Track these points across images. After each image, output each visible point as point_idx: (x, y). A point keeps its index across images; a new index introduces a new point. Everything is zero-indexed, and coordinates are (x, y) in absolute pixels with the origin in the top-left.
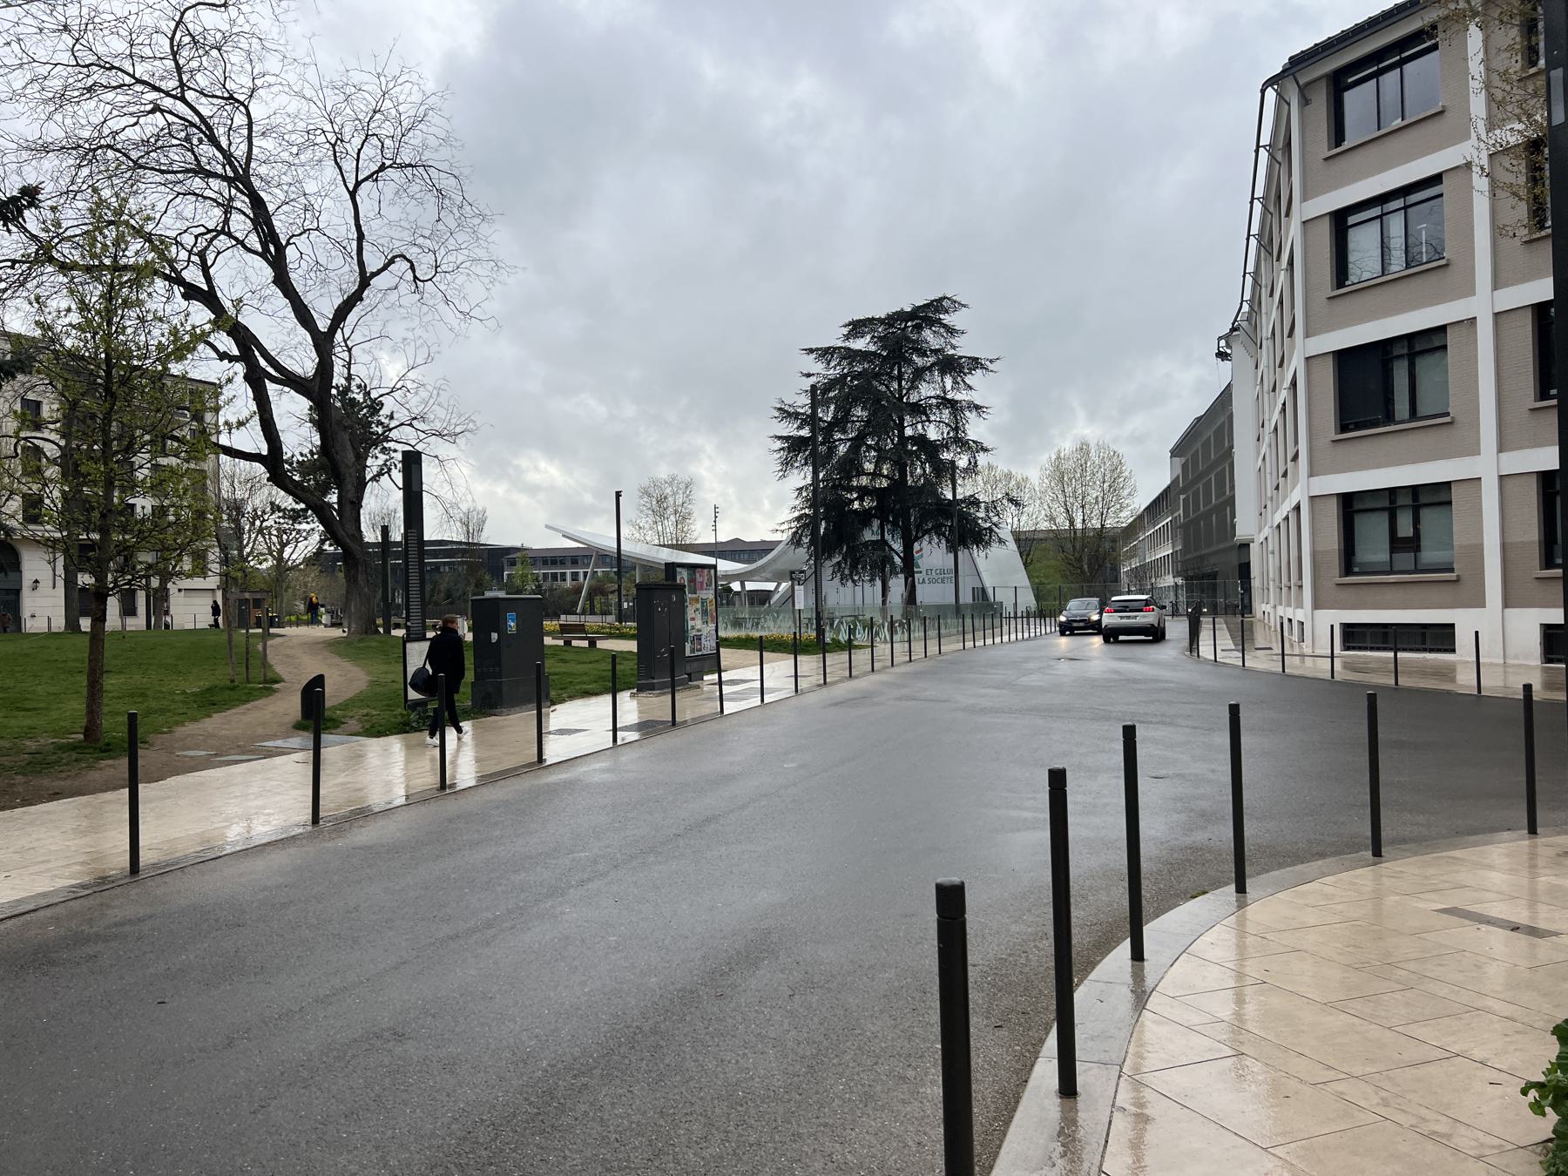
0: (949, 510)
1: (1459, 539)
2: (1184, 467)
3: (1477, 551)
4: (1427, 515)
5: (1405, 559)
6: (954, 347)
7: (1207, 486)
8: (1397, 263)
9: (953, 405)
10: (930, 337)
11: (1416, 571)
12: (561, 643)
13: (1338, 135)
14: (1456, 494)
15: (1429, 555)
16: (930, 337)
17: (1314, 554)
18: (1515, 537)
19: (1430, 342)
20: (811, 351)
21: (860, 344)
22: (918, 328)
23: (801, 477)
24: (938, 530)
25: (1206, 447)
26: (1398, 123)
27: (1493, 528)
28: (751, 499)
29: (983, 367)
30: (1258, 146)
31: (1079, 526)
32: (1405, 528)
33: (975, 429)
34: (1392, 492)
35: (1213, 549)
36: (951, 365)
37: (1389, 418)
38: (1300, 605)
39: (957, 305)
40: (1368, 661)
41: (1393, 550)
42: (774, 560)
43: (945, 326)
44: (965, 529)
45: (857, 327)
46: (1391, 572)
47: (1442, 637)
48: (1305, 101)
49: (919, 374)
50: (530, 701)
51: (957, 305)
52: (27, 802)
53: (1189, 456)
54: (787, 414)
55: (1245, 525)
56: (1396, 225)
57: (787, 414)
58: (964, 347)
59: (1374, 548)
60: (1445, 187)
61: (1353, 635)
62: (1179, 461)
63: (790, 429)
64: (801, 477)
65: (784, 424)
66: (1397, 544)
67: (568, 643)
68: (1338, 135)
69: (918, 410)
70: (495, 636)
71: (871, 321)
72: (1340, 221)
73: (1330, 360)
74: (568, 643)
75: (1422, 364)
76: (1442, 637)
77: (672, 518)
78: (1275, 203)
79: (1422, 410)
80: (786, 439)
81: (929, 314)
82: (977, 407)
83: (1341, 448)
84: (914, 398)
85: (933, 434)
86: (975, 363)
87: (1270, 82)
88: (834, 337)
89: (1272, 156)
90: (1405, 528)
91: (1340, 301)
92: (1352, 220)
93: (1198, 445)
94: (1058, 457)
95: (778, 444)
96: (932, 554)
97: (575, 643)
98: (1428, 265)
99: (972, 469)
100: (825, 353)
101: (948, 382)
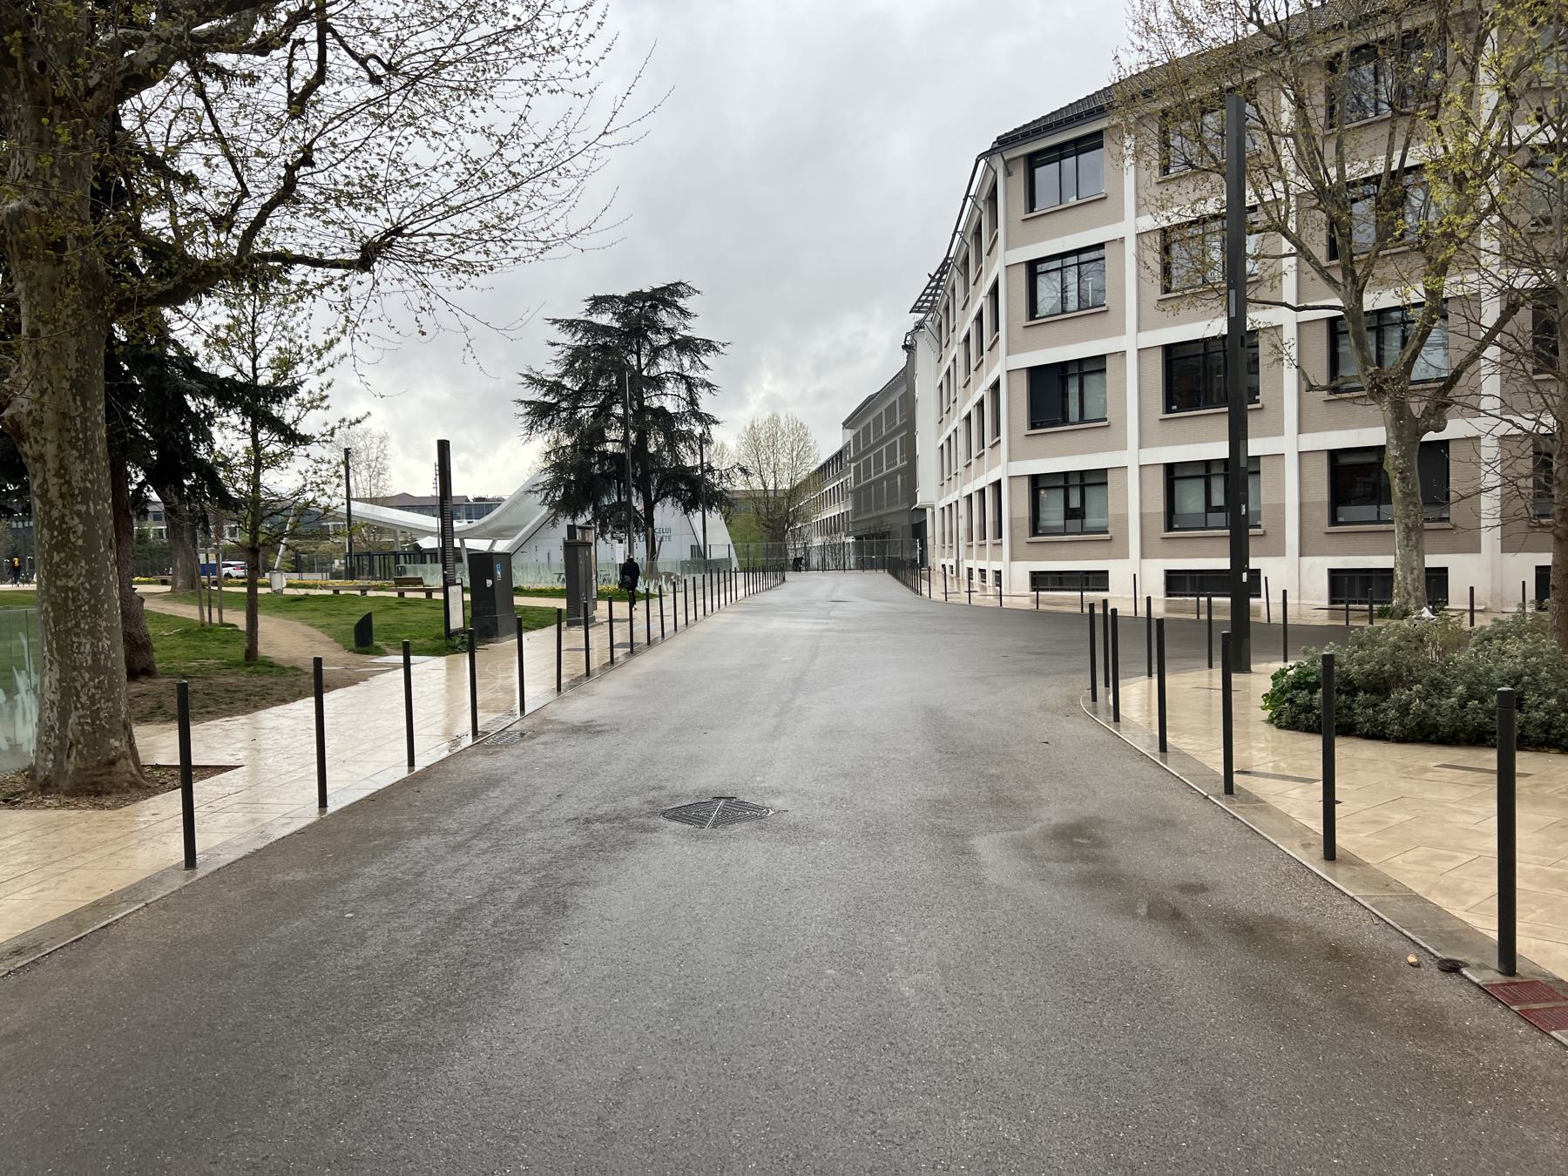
0: (684, 474)
1: (1112, 509)
2: (856, 437)
3: (1124, 520)
4: (1089, 492)
5: (1074, 524)
6: (685, 328)
7: (878, 457)
8: (1073, 304)
9: (690, 385)
10: (665, 317)
11: (1082, 533)
12: (396, 594)
13: (1031, 205)
14: (1110, 477)
15: (1092, 521)
16: (665, 317)
17: (1011, 520)
18: (1148, 509)
19: (1097, 364)
20: (555, 321)
21: (605, 319)
22: (654, 307)
23: (541, 443)
24: (676, 493)
25: (885, 421)
26: (1073, 200)
27: (1133, 501)
28: (509, 464)
29: (715, 349)
30: (967, 195)
31: (771, 487)
32: (1075, 502)
33: (706, 403)
34: (1066, 474)
35: (894, 509)
36: (687, 345)
37: (1065, 420)
38: (1000, 559)
39: (692, 291)
40: (1053, 598)
41: (1067, 517)
42: (496, 518)
43: (678, 308)
44: (696, 492)
45: (598, 303)
46: (1065, 533)
47: (1098, 580)
48: (1008, 174)
49: (656, 352)
50: (509, 632)
51: (692, 291)
52: (284, 701)
53: (860, 428)
54: (533, 381)
55: (928, 492)
56: (1072, 277)
57: (533, 381)
58: (697, 329)
59: (1053, 513)
60: (1105, 252)
61: (1039, 581)
62: (850, 434)
63: (537, 395)
64: (541, 443)
65: (530, 390)
66: (1071, 514)
67: (401, 595)
68: (1031, 205)
69: (657, 383)
70: (489, 582)
71: (609, 299)
72: (1032, 267)
73: (1025, 373)
74: (401, 595)
75: (1091, 381)
76: (1098, 580)
77: (365, 473)
78: (976, 236)
79: (1089, 415)
80: (530, 403)
81: (665, 296)
82: (709, 385)
83: (1030, 441)
84: (654, 372)
85: (671, 408)
86: (709, 346)
87: (983, 156)
88: (578, 311)
89: (975, 204)
90: (1075, 502)
91: (1036, 329)
92: (1040, 268)
93: (870, 419)
94: (753, 427)
95: (522, 410)
96: (667, 515)
97: (407, 595)
98: (1092, 308)
99: (704, 440)
100: (570, 325)
101: (686, 362)
